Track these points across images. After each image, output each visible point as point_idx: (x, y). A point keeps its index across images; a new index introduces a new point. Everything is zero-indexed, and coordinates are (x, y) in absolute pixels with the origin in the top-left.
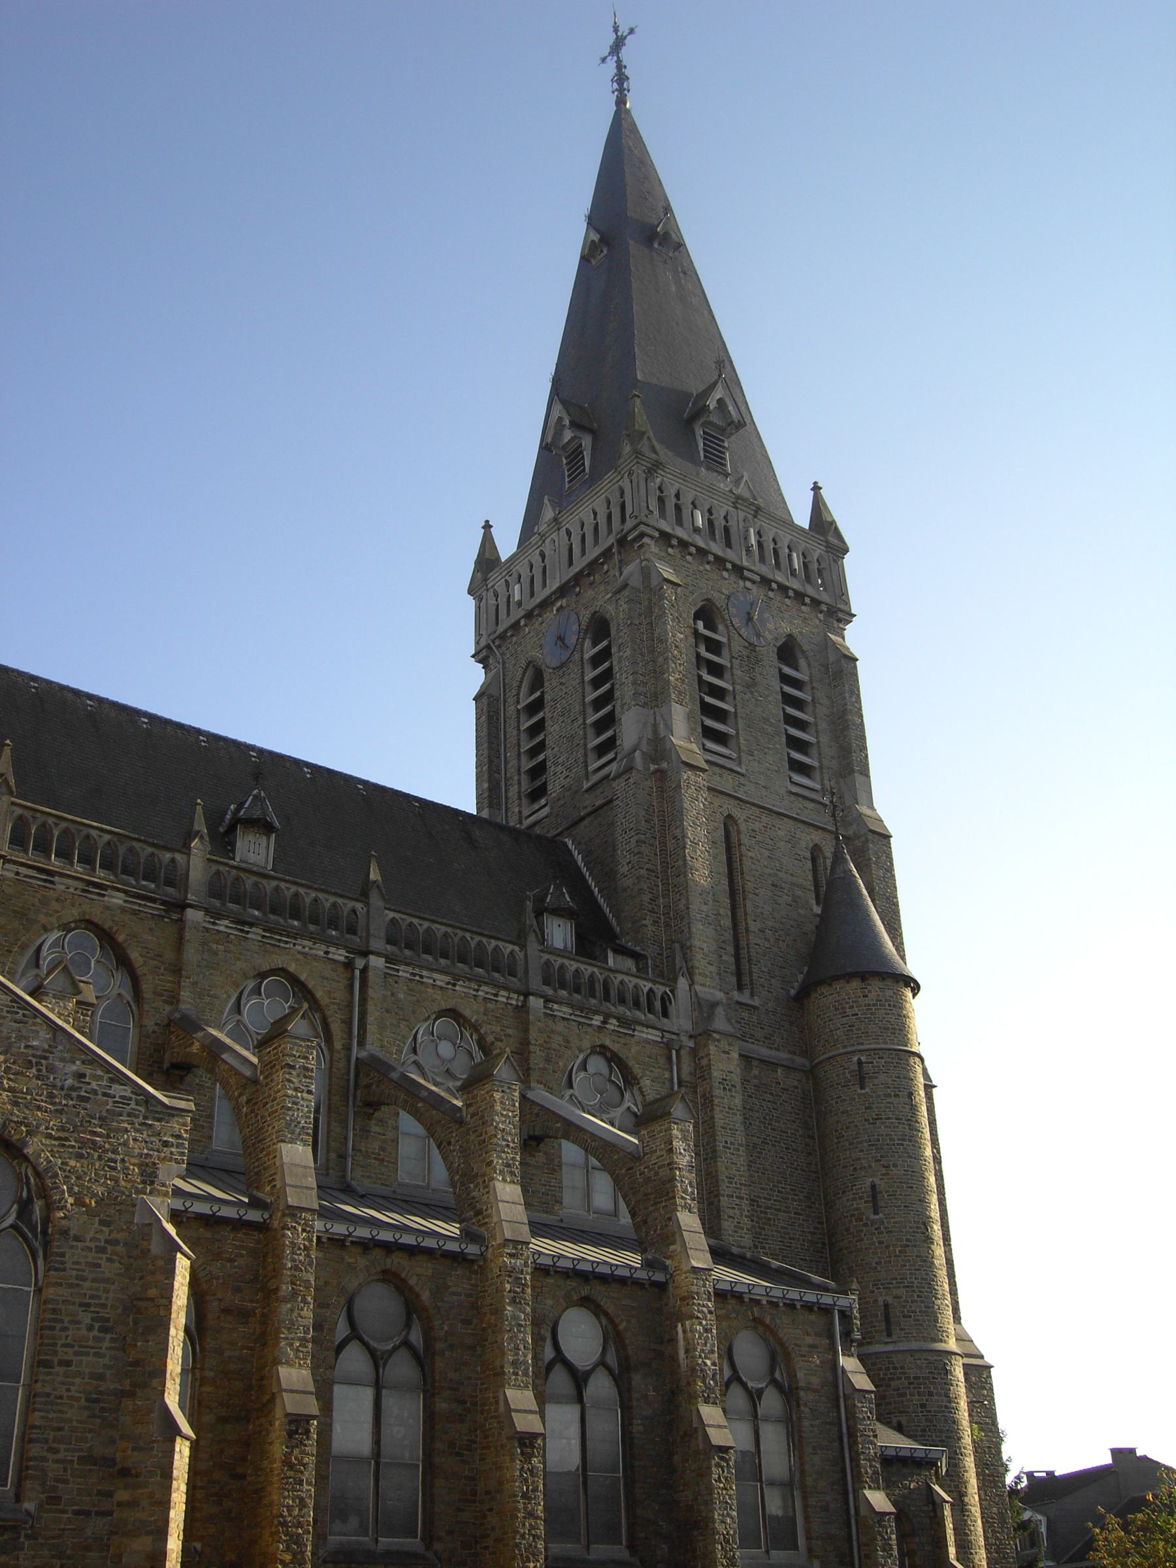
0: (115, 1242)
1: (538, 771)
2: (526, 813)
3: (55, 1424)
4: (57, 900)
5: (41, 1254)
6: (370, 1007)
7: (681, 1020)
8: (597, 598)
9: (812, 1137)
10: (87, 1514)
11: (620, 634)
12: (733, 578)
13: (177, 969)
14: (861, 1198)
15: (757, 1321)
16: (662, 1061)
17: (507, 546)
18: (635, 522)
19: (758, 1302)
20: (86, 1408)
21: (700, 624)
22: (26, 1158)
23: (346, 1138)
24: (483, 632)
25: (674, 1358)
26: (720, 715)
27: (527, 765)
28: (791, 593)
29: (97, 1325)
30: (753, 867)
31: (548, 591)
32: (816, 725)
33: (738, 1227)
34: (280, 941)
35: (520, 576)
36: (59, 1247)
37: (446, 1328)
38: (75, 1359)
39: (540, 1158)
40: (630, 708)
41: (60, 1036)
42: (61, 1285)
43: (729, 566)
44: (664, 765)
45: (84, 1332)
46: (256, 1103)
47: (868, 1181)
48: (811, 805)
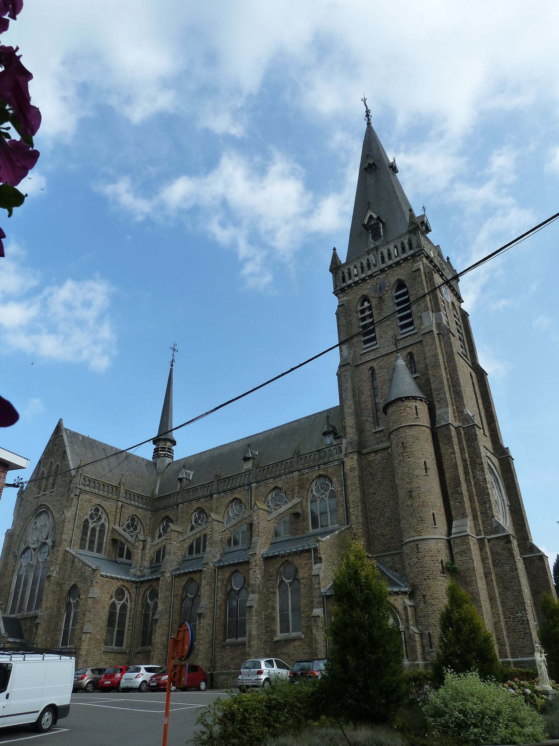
33: (357, 517)
48: (409, 338)
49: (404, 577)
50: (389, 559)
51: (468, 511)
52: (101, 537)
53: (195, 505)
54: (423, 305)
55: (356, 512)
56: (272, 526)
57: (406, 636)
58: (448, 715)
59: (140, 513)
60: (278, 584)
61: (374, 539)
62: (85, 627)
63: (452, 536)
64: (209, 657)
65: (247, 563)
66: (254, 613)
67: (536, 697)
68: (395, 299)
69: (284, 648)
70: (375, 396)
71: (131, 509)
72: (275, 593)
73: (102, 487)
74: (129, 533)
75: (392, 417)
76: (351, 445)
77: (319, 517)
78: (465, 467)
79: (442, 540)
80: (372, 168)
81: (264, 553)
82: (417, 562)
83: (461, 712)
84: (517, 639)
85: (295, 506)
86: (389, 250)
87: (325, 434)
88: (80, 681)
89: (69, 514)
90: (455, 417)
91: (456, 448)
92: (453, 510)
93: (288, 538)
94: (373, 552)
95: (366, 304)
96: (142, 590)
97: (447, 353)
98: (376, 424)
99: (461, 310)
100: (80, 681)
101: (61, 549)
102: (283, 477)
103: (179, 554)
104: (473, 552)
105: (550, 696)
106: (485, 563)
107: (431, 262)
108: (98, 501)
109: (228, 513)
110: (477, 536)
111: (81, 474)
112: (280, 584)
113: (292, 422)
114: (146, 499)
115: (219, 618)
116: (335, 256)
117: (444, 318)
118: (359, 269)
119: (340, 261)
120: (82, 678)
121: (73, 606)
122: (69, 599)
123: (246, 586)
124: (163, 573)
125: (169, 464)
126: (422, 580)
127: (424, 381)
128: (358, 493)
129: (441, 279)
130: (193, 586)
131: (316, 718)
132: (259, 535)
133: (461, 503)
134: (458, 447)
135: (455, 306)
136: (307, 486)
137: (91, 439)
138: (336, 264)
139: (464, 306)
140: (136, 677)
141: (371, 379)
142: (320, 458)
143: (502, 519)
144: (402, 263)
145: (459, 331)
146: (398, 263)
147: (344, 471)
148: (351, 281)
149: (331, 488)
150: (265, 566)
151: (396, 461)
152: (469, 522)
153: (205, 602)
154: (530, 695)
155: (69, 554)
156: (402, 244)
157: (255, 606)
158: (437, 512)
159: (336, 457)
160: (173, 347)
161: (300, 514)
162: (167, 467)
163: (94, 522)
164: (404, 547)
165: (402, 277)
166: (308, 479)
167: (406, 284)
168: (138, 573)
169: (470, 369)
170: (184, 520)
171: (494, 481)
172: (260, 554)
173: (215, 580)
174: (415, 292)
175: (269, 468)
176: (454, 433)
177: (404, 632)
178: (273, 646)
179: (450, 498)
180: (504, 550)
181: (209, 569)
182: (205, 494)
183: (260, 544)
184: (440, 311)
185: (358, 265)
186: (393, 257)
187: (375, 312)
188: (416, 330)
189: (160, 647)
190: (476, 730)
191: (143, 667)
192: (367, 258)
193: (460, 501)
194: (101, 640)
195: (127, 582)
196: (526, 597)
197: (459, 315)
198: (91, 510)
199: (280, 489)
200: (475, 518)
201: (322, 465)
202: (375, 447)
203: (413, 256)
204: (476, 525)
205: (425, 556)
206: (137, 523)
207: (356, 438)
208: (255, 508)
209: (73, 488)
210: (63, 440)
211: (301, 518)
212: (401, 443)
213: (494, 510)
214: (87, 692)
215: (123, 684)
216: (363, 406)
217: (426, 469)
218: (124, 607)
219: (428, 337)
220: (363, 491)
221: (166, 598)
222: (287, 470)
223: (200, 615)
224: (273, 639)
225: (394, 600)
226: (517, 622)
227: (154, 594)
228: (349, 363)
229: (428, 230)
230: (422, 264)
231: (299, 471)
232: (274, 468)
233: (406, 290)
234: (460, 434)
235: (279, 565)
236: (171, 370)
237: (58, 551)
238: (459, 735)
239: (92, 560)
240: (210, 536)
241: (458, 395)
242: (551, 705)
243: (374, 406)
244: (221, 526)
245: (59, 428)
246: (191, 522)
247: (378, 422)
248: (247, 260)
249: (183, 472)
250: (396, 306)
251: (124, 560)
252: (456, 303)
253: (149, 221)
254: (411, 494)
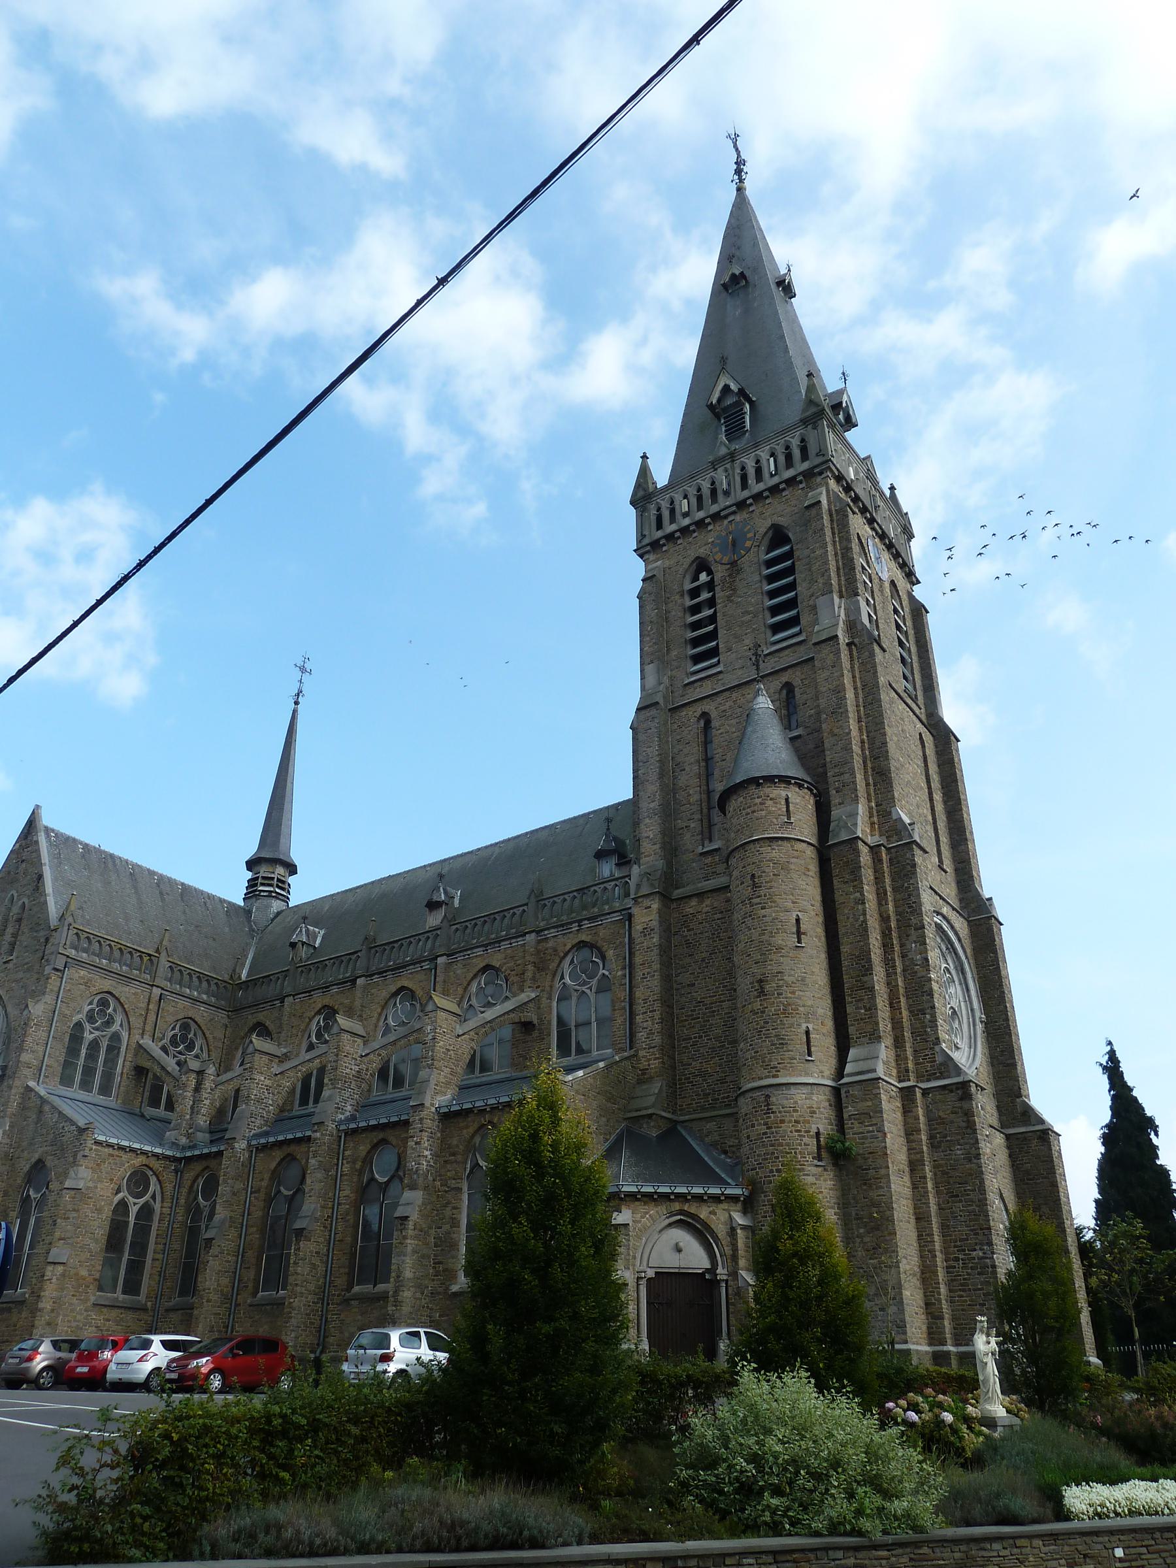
33: (651, 1033)
48: (786, 652)
49: (736, 1168)
50: (711, 1125)
51: (885, 1025)
52: (111, 1061)
53: (319, 1000)
54: (821, 580)
55: (649, 1024)
56: (465, 1048)
57: (730, 1291)
58: (724, 1465)
59: (201, 1014)
60: (467, 1172)
61: (684, 1083)
62: (54, 1251)
63: (842, 1081)
64: (313, 1323)
65: (406, 1123)
66: (410, 1232)
67: (965, 1430)
68: (763, 568)
70: (709, 775)
71: (182, 1003)
72: (460, 1190)
73: (117, 954)
74: (175, 1056)
75: (734, 821)
76: (648, 879)
77: (573, 1034)
78: (886, 934)
79: (823, 1087)
80: (738, 283)
81: (444, 1104)
82: (764, 1134)
83: (754, 1459)
84: (969, 1305)
85: (522, 1007)
86: (758, 462)
87: (600, 855)
88: (24, 1365)
89: (38, 1009)
90: (872, 824)
91: (868, 892)
92: (852, 1025)
93: (504, 1076)
94: (680, 1110)
95: (703, 577)
96: (189, 1176)
97: (864, 686)
98: (707, 834)
99: (911, 598)
100: (24, 1365)
101: (17, 1083)
102: (505, 945)
103: (270, 1102)
104: (885, 1116)
105: (999, 1429)
106: (913, 1141)
107: (848, 489)
108: (107, 984)
109: (386, 1019)
110: (900, 1081)
111: (70, 925)
112: (471, 1172)
113: (537, 830)
114: (216, 984)
115: (342, 1241)
116: (644, 472)
117: (864, 609)
118: (694, 501)
119: (654, 483)
120: (30, 1359)
121: (34, 1204)
122: (28, 1191)
123: (401, 1173)
124: (230, 1142)
125: (279, 913)
126: (772, 1171)
127: (811, 746)
128: (655, 983)
129: (868, 529)
130: (293, 1172)
131: (395, 1462)
132: (432, 1065)
133: (870, 1009)
134: (874, 889)
135: (897, 591)
136: (553, 966)
137: (105, 852)
138: (645, 490)
139: (918, 592)
140: (140, 1360)
141: (701, 738)
142: (584, 907)
143: (967, 1049)
144: (784, 489)
145: (901, 644)
146: (774, 490)
147: (630, 935)
148: (674, 527)
149: (601, 972)
150: (442, 1131)
151: (736, 916)
152: (885, 1051)
153: (313, 1206)
154: (950, 1426)
155: (33, 1094)
156: (787, 448)
157: (414, 1216)
158: (816, 1027)
159: (617, 905)
160: (300, 663)
161: (534, 1025)
162: (273, 920)
163: (97, 1029)
164: (742, 1100)
165: (782, 521)
166: (555, 950)
167: (790, 535)
168: (184, 1141)
169: (919, 725)
170: (294, 1031)
171: (956, 968)
172: (432, 1105)
173: (338, 1159)
174: (807, 552)
175: (476, 924)
176: (865, 857)
177: (726, 1284)
178: (448, 1302)
179: (849, 999)
180: (956, 1113)
181: (326, 1135)
182: (341, 977)
183: (436, 1085)
184: (857, 594)
185: (692, 492)
186: (766, 475)
187: (720, 594)
188: (804, 634)
189: (214, 1297)
190: (775, 1501)
191: (156, 1339)
192: (712, 477)
193: (868, 1006)
194: (90, 1279)
195: (155, 1158)
196: (996, 1215)
197: (907, 610)
198: (91, 1004)
199: (497, 970)
200: (898, 1043)
201: (586, 922)
202: (700, 885)
203: (809, 475)
204: (900, 1058)
205: (782, 1122)
206: (195, 1035)
207: (660, 864)
208: (430, 1007)
209: (52, 953)
210: (38, 851)
211: (536, 1034)
212: (749, 877)
213: (940, 1028)
214: (40, 1388)
215: (113, 1373)
216: (681, 796)
217: (799, 933)
218: (146, 1212)
219: (826, 649)
220: (667, 979)
221: (234, 1194)
222: (514, 931)
223: (300, 1233)
224: (447, 1289)
225: (710, 1213)
226: (972, 1268)
227: (211, 1188)
228: (657, 703)
229: (850, 423)
230: (825, 493)
231: (538, 932)
232: (486, 927)
233: (787, 548)
234: (881, 861)
235: (471, 1130)
236: (295, 712)
237: (10, 1087)
238: (743, 1510)
239: (86, 1109)
240: (333, 1064)
241: (881, 776)
242: (995, 1449)
243: (704, 796)
244: (358, 1045)
245: (32, 825)
246: (309, 1036)
247: (710, 832)
248: (427, 459)
249: (301, 931)
250: (765, 582)
251: (161, 1112)
252: (902, 583)
253: (206, 361)
254: (762, 988)
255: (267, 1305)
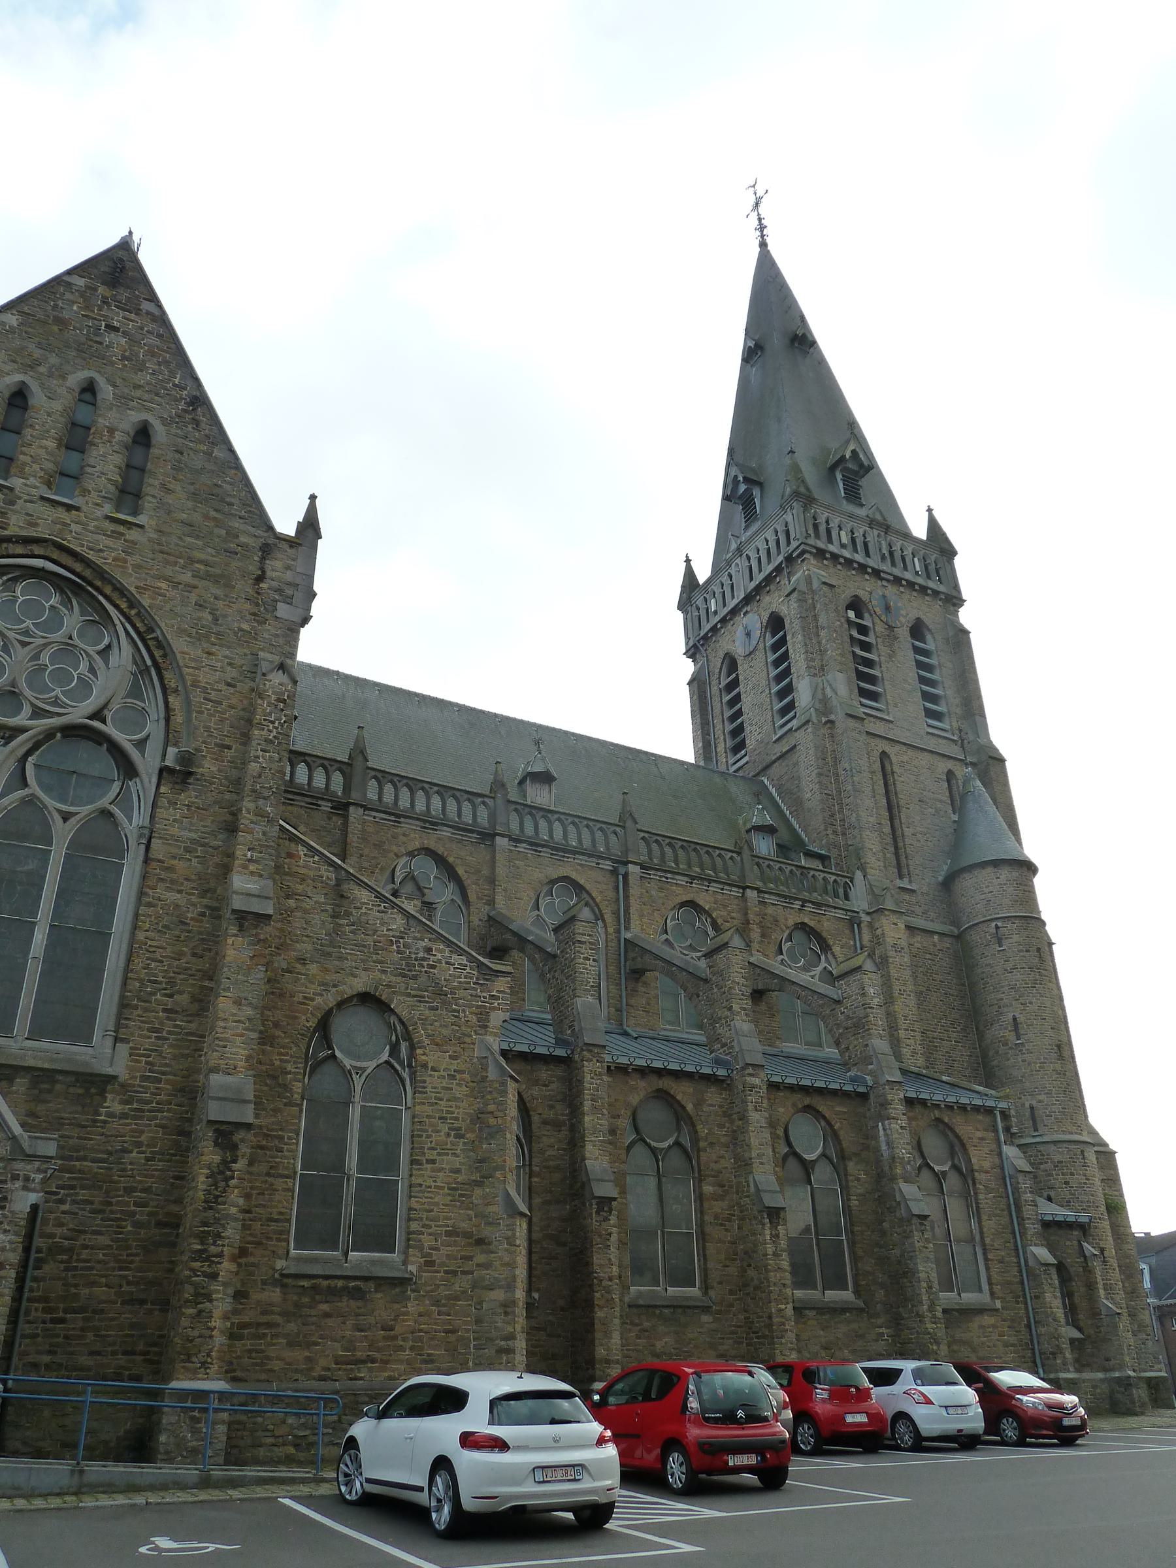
0: (463, 1072)
1: (739, 730)
2: (731, 762)
3: (426, 1206)
4: (404, 835)
5: (408, 1082)
6: (632, 901)
7: (860, 901)
8: (774, 602)
9: (963, 985)
10: (454, 1273)
11: (793, 626)
12: (873, 580)
13: (492, 881)
14: (1005, 1029)
15: (938, 1120)
16: (847, 932)
17: (703, 573)
18: (797, 543)
19: (938, 1106)
20: (449, 1195)
21: (851, 614)
22: (392, 1010)
23: (621, 996)
24: (690, 635)
25: (877, 1150)
26: (872, 680)
27: (729, 727)
28: (917, 587)
29: (453, 1133)
30: (904, 788)
31: (736, 601)
32: (943, 682)
33: (914, 1053)
34: (564, 857)
35: (714, 593)
36: (421, 1076)
37: (706, 1131)
38: (438, 1158)
39: (763, 1006)
40: (803, 678)
41: (412, 922)
42: (424, 1104)
43: (869, 570)
44: (832, 717)
45: (444, 1138)
46: (555, 971)
47: (1011, 1015)
48: (944, 742)
69: (959, 1327)
102: (714, 887)
201: (810, 905)
255: (667, 1307)
